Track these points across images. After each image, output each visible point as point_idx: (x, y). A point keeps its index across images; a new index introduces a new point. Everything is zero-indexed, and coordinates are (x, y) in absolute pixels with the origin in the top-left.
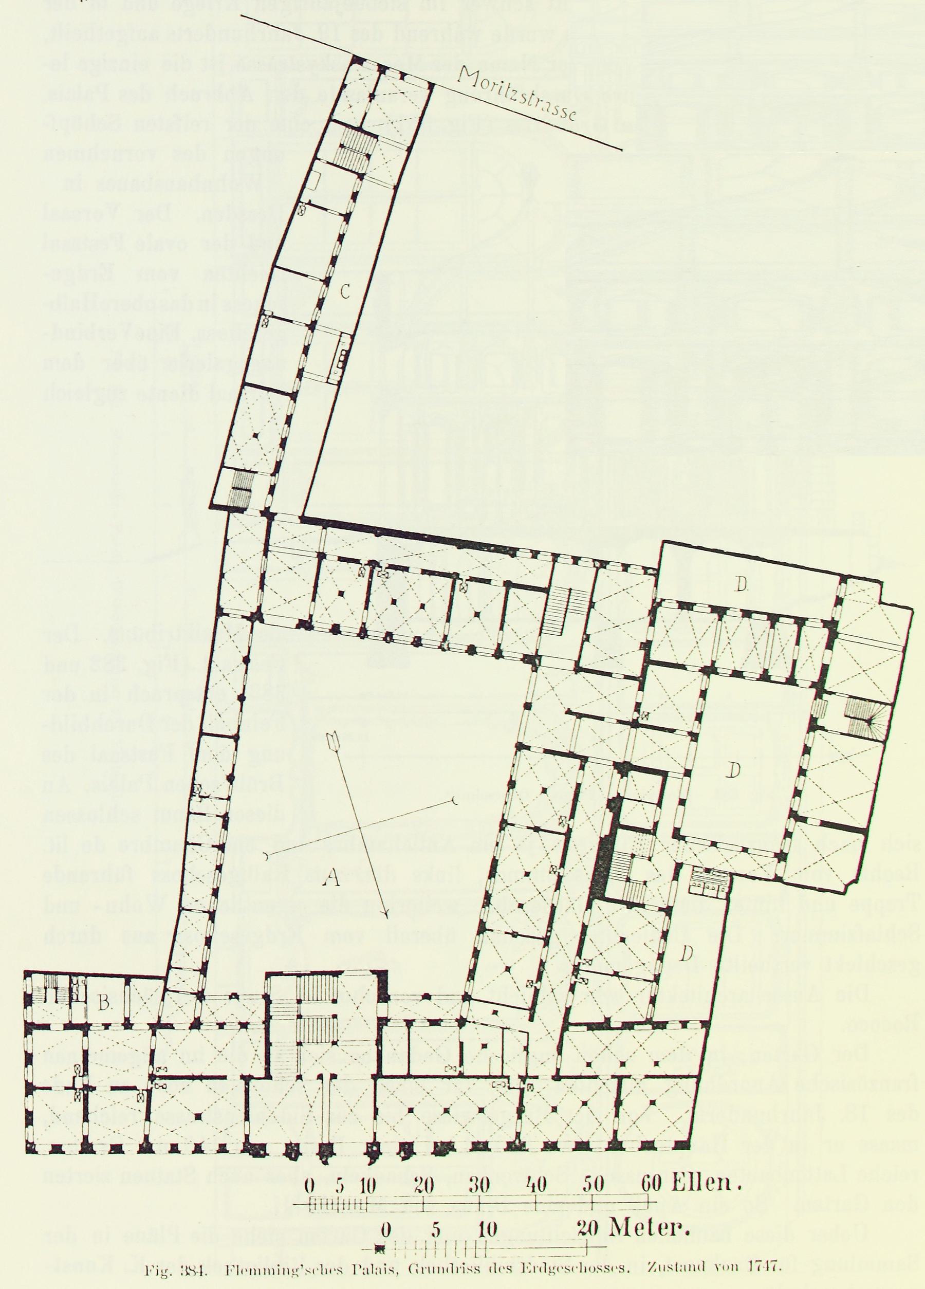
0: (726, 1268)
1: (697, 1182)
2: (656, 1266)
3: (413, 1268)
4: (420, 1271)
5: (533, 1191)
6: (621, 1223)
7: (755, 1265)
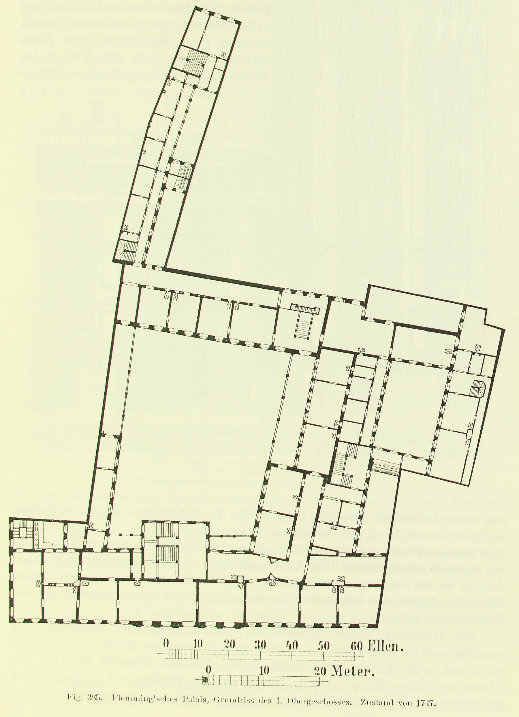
0: (405, 704)
1: (381, 645)
3: (217, 699)
4: (220, 701)
5: (290, 649)
6: (338, 668)
7: (421, 703)
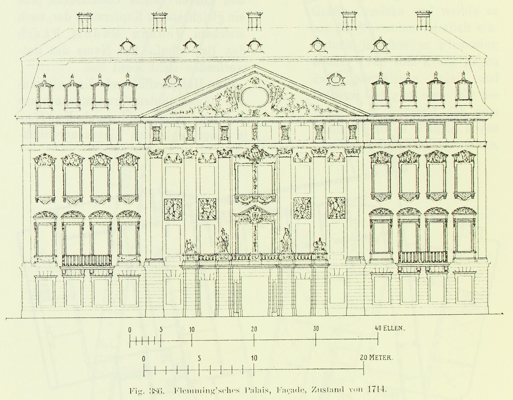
0: (356, 390)
2: (316, 389)
